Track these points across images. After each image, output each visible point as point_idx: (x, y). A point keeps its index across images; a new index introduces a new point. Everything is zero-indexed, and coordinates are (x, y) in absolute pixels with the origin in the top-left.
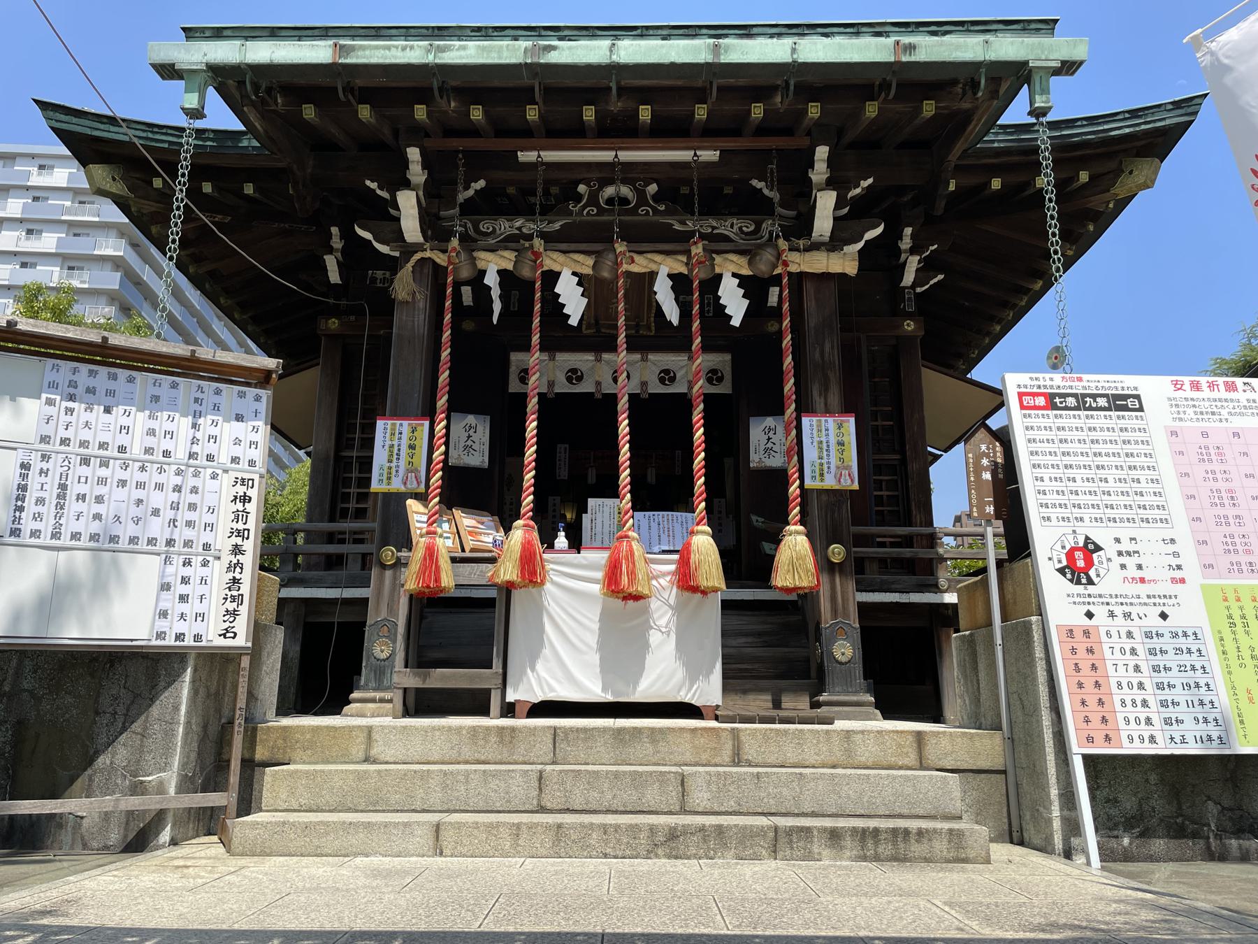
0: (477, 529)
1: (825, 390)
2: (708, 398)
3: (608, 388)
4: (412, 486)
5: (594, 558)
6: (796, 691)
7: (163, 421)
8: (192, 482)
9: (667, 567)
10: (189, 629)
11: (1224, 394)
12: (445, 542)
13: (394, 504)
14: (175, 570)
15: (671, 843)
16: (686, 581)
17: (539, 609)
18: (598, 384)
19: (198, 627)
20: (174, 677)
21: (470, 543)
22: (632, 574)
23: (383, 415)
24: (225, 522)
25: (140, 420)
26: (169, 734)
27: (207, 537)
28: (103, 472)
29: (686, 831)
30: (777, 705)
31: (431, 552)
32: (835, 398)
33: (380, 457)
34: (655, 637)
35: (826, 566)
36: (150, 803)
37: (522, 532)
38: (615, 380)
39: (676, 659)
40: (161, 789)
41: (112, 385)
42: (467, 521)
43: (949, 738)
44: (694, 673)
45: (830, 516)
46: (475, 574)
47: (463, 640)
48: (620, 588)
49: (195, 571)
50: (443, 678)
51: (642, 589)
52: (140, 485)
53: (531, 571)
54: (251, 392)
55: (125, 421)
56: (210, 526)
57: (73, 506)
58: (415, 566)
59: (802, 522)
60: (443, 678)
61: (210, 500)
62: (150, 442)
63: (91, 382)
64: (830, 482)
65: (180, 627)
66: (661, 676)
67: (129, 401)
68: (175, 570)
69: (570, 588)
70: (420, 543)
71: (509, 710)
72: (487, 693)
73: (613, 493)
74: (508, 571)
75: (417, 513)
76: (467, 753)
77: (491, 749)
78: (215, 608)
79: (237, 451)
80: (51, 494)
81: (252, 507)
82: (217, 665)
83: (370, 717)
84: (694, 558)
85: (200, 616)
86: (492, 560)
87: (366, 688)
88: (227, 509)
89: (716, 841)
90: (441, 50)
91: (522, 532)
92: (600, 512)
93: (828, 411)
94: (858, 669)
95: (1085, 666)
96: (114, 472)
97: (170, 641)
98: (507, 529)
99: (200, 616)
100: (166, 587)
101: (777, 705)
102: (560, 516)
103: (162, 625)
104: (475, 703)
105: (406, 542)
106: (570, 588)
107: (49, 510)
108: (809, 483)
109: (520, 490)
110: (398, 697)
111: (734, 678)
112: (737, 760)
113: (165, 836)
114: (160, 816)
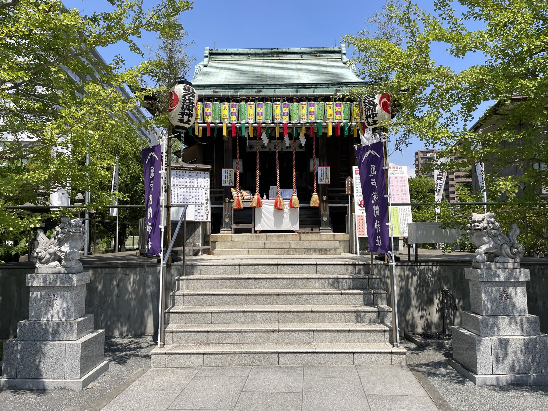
0: (247, 195)
1: (323, 161)
2: (297, 153)
3: (273, 150)
4: (231, 184)
5: (272, 201)
6: (316, 227)
7: (192, 180)
8: (198, 191)
9: (287, 203)
10: (201, 218)
11: (395, 169)
12: (240, 197)
13: (228, 189)
14: (197, 208)
15: (288, 252)
16: (291, 205)
17: (261, 211)
18: (270, 149)
19: (202, 218)
20: (199, 226)
21: (245, 198)
22: (280, 205)
23: (223, 168)
24: (204, 199)
25: (188, 180)
26: (199, 236)
27: (201, 201)
28: (184, 190)
29: (290, 251)
30: (312, 230)
31: (238, 200)
32: (325, 163)
33: (223, 178)
34: (285, 215)
35: (321, 200)
36: (198, 248)
37: (257, 196)
38: (275, 148)
39: (289, 221)
40: (198, 245)
41: (183, 174)
42: (244, 193)
43: (340, 236)
44: (293, 225)
45: (322, 190)
46: (248, 205)
47: (245, 218)
48: (278, 208)
49: (200, 208)
50: (242, 226)
51: (282, 207)
52: (190, 192)
53: (259, 204)
54: (206, 173)
55: (186, 180)
56: (202, 199)
57: (180, 197)
58: (235, 203)
59: (317, 192)
60: (242, 226)
61: (201, 194)
62: (190, 184)
63: (179, 173)
64: (324, 182)
65: (199, 218)
66: (286, 225)
67: (186, 177)
68: (197, 208)
69: (267, 207)
70: (235, 199)
71: (255, 232)
72: (251, 229)
73: (275, 184)
74: (254, 204)
75: (234, 192)
76: (250, 239)
77: (255, 239)
78: (204, 214)
79: (205, 185)
80: (176, 195)
81: (208, 195)
82: (204, 224)
83: (225, 233)
84: (293, 201)
85: (202, 216)
86: (251, 202)
87: (224, 228)
88: (204, 196)
89: (295, 252)
90: (237, 92)
91: (257, 196)
92: (273, 189)
93: (324, 166)
94: (328, 223)
95: (361, 222)
96: (185, 190)
97: (198, 220)
98: (253, 195)
99: (202, 216)
100: (196, 211)
101: (312, 230)
102: (264, 192)
103: (196, 217)
104: (248, 231)
105: (231, 197)
106: (267, 207)
107: (176, 198)
108: (319, 182)
109: (256, 187)
110: (233, 229)
111: (302, 224)
112: (300, 240)
113: (200, 253)
114: (199, 250)
